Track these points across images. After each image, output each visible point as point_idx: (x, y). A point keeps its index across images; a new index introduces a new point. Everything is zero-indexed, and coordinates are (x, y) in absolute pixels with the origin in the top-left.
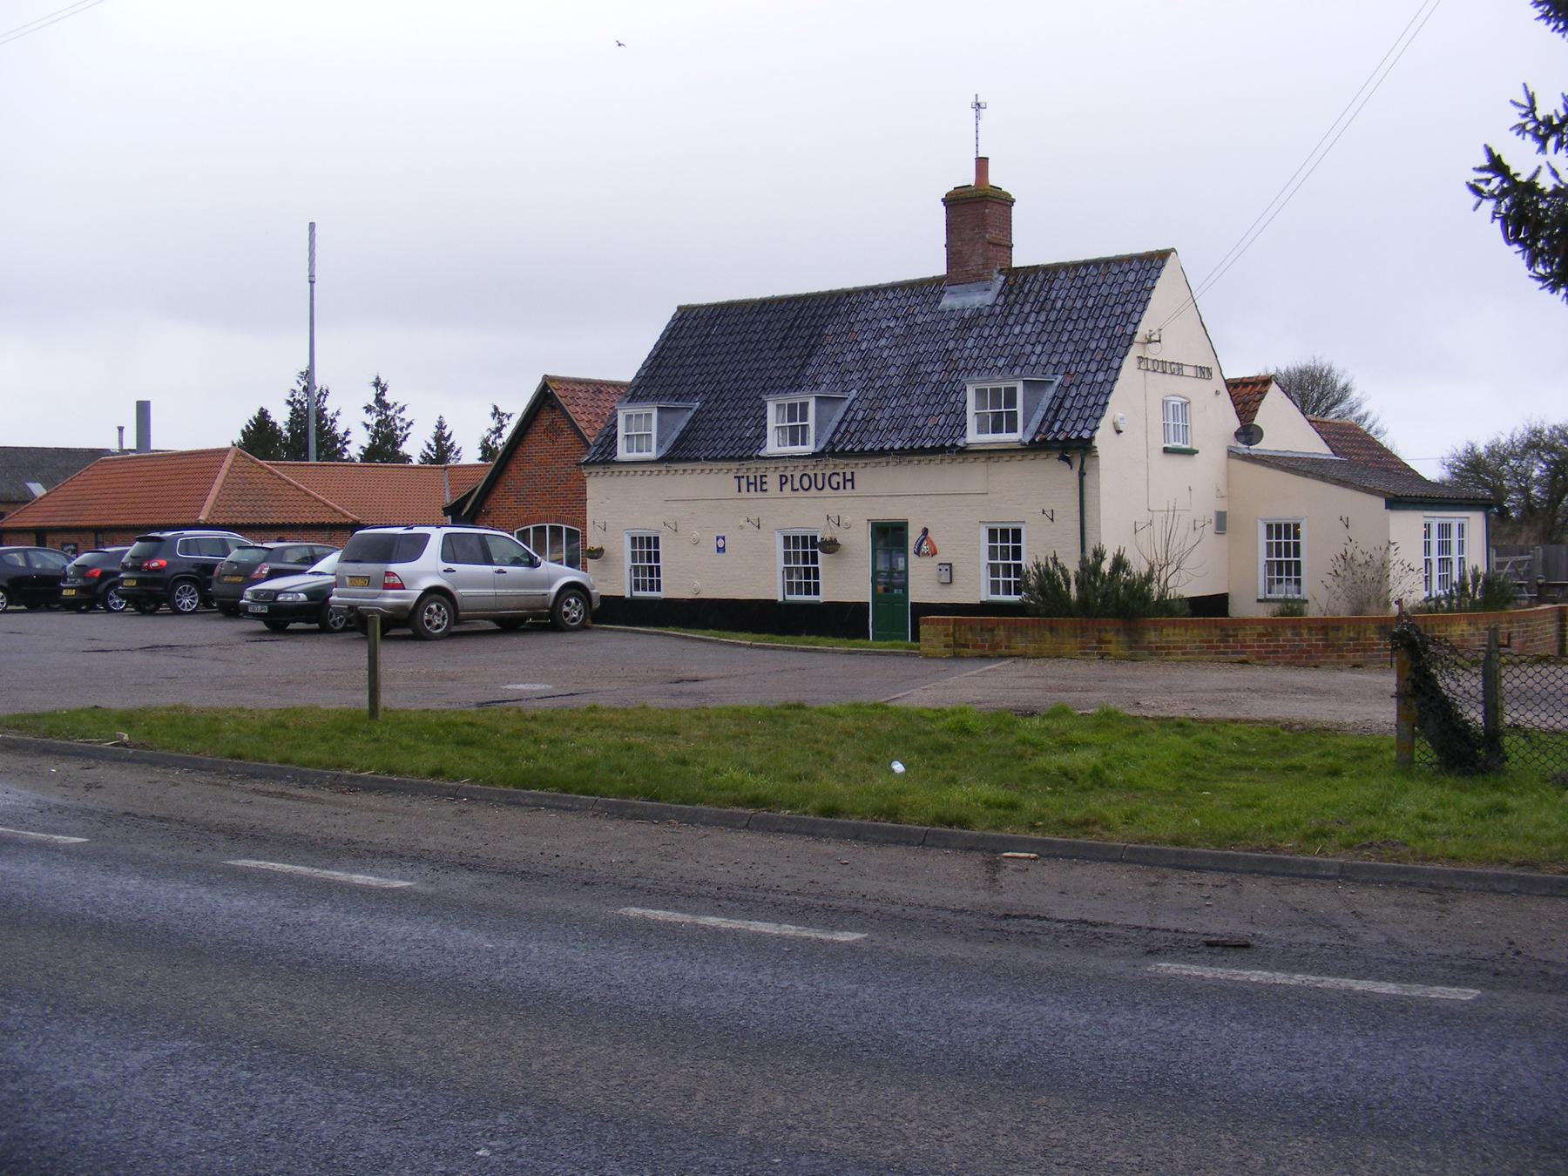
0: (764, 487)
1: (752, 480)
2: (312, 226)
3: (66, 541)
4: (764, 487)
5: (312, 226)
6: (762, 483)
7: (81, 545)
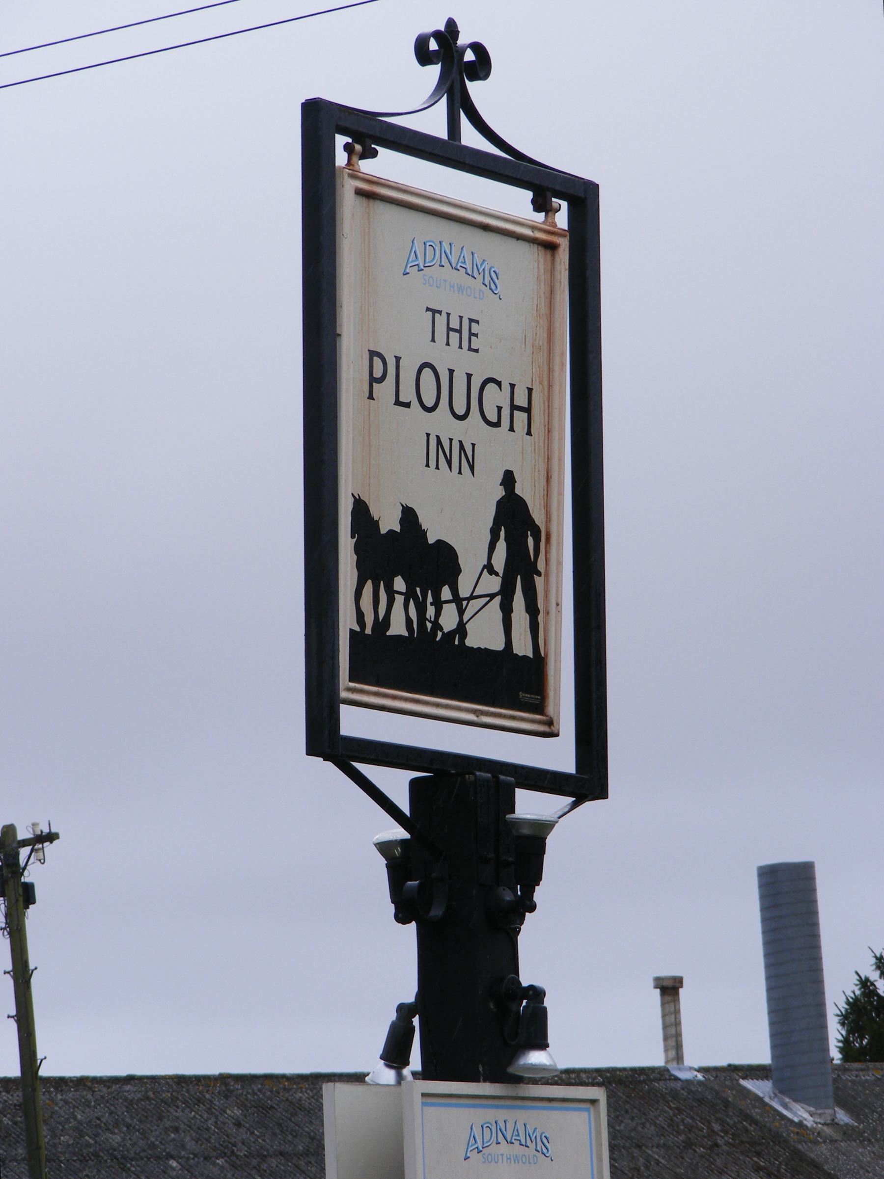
1: (454, 324)
6: (471, 334)
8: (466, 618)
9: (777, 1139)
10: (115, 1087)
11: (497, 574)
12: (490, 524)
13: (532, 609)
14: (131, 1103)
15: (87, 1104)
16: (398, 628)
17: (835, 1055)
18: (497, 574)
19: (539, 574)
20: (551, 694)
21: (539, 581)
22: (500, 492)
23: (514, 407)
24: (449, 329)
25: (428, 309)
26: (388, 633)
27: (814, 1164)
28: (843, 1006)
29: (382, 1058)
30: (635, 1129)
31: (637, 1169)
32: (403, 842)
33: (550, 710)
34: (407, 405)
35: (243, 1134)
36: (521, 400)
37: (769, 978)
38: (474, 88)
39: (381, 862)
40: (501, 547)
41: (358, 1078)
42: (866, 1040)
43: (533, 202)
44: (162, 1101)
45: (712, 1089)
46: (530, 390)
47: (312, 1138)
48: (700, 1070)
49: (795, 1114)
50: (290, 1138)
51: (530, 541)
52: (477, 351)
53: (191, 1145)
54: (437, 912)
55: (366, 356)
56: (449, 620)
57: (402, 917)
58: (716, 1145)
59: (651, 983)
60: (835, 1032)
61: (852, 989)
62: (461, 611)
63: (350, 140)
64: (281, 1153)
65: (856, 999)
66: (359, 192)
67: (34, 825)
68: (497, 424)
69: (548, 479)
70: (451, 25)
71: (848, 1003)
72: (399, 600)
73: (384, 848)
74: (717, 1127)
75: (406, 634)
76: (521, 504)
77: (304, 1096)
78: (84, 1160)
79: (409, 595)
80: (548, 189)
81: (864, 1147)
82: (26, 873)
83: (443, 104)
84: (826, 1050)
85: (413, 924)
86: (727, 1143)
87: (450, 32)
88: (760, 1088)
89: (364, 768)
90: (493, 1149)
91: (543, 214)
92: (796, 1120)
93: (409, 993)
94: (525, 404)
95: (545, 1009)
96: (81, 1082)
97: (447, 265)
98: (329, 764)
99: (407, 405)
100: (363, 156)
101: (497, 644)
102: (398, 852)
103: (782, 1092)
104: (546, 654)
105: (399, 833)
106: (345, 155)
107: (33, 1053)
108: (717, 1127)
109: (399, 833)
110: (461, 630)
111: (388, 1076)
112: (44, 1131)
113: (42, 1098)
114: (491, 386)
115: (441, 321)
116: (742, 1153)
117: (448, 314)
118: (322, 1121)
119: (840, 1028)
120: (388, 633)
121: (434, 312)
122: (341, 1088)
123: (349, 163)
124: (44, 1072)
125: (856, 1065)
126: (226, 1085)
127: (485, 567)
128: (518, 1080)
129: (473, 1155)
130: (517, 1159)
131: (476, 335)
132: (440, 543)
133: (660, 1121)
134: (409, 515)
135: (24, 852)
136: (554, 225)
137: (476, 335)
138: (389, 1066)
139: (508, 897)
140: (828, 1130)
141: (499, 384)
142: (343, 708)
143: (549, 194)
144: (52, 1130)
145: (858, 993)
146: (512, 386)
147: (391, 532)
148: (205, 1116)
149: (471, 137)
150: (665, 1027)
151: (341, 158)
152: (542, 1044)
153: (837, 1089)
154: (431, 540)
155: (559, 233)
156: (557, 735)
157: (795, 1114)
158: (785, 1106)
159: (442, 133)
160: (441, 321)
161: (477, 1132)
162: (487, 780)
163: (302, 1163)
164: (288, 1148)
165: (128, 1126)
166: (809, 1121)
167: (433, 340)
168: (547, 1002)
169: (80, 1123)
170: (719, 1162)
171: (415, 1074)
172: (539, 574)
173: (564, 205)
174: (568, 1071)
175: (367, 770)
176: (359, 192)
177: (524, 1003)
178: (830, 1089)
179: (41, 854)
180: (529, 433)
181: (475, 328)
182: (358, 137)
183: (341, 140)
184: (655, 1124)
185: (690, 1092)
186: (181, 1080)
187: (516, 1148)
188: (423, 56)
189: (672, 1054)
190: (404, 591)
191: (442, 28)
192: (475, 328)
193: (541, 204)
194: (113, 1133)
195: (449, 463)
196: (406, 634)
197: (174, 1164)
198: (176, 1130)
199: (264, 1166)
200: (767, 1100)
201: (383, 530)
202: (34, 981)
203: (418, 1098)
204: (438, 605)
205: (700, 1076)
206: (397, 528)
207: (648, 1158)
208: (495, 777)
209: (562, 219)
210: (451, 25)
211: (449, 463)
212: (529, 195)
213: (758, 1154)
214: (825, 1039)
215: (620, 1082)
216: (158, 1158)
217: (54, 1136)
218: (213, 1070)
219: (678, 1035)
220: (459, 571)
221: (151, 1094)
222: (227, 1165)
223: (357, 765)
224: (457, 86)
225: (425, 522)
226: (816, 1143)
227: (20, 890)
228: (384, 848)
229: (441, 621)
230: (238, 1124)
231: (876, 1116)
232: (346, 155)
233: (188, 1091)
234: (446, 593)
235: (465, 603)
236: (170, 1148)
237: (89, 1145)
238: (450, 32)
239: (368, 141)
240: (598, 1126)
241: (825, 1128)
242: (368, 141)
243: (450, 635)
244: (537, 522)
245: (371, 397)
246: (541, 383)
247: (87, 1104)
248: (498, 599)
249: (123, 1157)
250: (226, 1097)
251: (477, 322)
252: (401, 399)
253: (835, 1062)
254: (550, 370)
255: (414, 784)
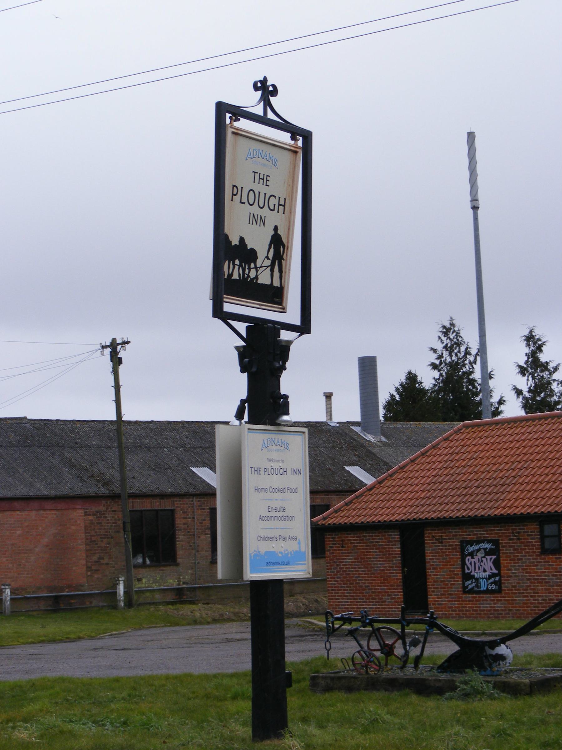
0: (268, 183)
1: (262, 177)
2: (471, 136)
3: (469, 538)
4: (268, 183)
5: (471, 136)
6: (267, 180)
7: (504, 541)
8: (258, 273)
9: (362, 446)
10: (147, 424)
11: (270, 260)
12: (269, 243)
13: (281, 271)
14: (152, 430)
15: (138, 430)
16: (235, 276)
17: (382, 419)
18: (270, 260)
19: (284, 260)
20: (285, 299)
21: (283, 262)
22: (273, 233)
23: (279, 205)
24: (260, 178)
25: (253, 172)
26: (232, 278)
27: (373, 454)
28: (385, 403)
29: (235, 417)
30: (316, 442)
31: (316, 455)
32: (244, 346)
33: (284, 304)
34: (244, 203)
35: (188, 441)
36: (282, 202)
37: (361, 394)
38: (272, 99)
39: (236, 353)
40: (272, 250)
41: (227, 423)
42: (471, 388)
43: (291, 137)
44: (162, 429)
45: (341, 429)
46: (285, 199)
47: (211, 442)
48: (337, 423)
49: (368, 438)
50: (204, 442)
51: (282, 249)
52: (268, 186)
53: (171, 444)
54: (254, 369)
55: (232, 187)
56: (253, 274)
57: (243, 371)
58: (342, 447)
59: (323, 395)
60: (382, 412)
61: (388, 398)
62: (257, 271)
63: (231, 115)
64: (201, 447)
65: (389, 401)
66: (233, 133)
67: (123, 338)
68: (273, 210)
69: (289, 229)
70: (265, 78)
71: (386, 402)
72: (237, 267)
73: (237, 348)
74: (342, 441)
75: (238, 278)
76: (280, 236)
77: (209, 428)
78: (136, 448)
79: (240, 266)
80: (296, 133)
81: (390, 449)
82: (119, 354)
83: (262, 104)
84: (379, 417)
85: (246, 373)
86: (346, 447)
87: (265, 80)
88: (357, 429)
89: (231, 322)
90: (271, 447)
91: (294, 141)
92: (368, 440)
93: (244, 396)
94: (283, 204)
95: (289, 402)
96: (136, 422)
97: (261, 157)
98: (220, 320)
99: (244, 203)
100: (235, 121)
101: (268, 282)
102: (242, 349)
103: (364, 431)
104: (284, 286)
105: (243, 343)
106: (229, 120)
107: (121, 413)
108: (342, 441)
109: (243, 343)
110: (257, 277)
111: (237, 423)
112: (124, 438)
113: (123, 427)
114: (272, 197)
115: (257, 175)
116: (350, 450)
117: (260, 174)
118: (215, 437)
119: (383, 410)
120: (232, 278)
121: (255, 173)
122: (221, 426)
123: (231, 123)
124: (123, 419)
125: (388, 422)
126: (183, 424)
127: (266, 257)
128: (279, 425)
129: (264, 449)
130: (278, 450)
131: (268, 181)
132: (252, 249)
133: (324, 439)
134: (242, 240)
135: (119, 347)
136: (297, 145)
137: (268, 181)
138: (238, 420)
139: (277, 365)
140: (378, 443)
141: (275, 197)
142: (224, 303)
143: (296, 135)
144: (126, 438)
145: (390, 399)
146: (279, 198)
147: (236, 245)
148: (176, 434)
149: (271, 115)
150: (327, 409)
151: (228, 121)
152: (287, 413)
153: (382, 430)
154: (249, 248)
155: (299, 148)
156: (286, 313)
157: (368, 438)
158: (365, 435)
159: (261, 113)
160: (257, 175)
161: (265, 441)
162: (271, 327)
163: (207, 450)
164: (202, 445)
165: (151, 437)
166: (373, 440)
167: (254, 182)
168: (289, 400)
169: (135, 436)
170: (343, 453)
171: (245, 422)
172: (284, 260)
173: (301, 138)
174: (294, 422)
175: (232, 322)
176: (233, 133)
177: (282, 400)
178: (379, 430)
179: (124, 348)
180: (284, 213)
181: (268, 178)
182: (234, 114)
183: (228, 115)
184: (323, 440)
185: (334, 430)
186: (169, 422)
187: (278, 447)
188: (256, 88)
189: (329, 418)
190: (238, 264)
191: (262, 79)
192: (268, 178)
193: (293, 138)
194: (146, 439)
195: (257, 223)
196: (238, 278)
197: (165, 449)
198: (167, 439)
199: (195, 451)
200: (359, 433)
201: (233, 244)
202: (121, 389)
203: (246, 430)
204: (250, 269)
205: (338, 425)
206: (238, 244)
207: (320, 451)
208: (274, 326)
209: (300, 143)
210: (265, 78)
211: (257, 223)
212: (289, 135)
213: (356, 450)
214: (378, 414)
215: (312, 426)
216: (161, 448)
217: (127, 440)
218: (180, 420)
219: (331, 411)
220: (257, 258)
221: (159, 427)
222: (183, 451)
223: (229, 321)
224: (267, 98)
225: (247, 242)
226: (374, 447)
227: (118, 360)
228: (237, 348)
229: (250, 275)
230: (187, 437)
231: (394, 439)
232: (229, 120)
233: (171, 426)
234: (252, 265)
235: (258, 269)
236: (164, 444)
237: (138, 443)
238: (265, 80)
239: (237, 116)
240: (305, 440)
241: (377, 442)
242: (237, 116)
243: (253, 279)
244: (284, 242)
245: (232, 200)
246: (289, 197)
247: (138, 430)
248: (270, 268)
249: (149, 447)
250: (183, 429)
251: (269, 176)
252: (242, 201)
253: (382, 421)
254: (292, 193)
255: (247, 327)
